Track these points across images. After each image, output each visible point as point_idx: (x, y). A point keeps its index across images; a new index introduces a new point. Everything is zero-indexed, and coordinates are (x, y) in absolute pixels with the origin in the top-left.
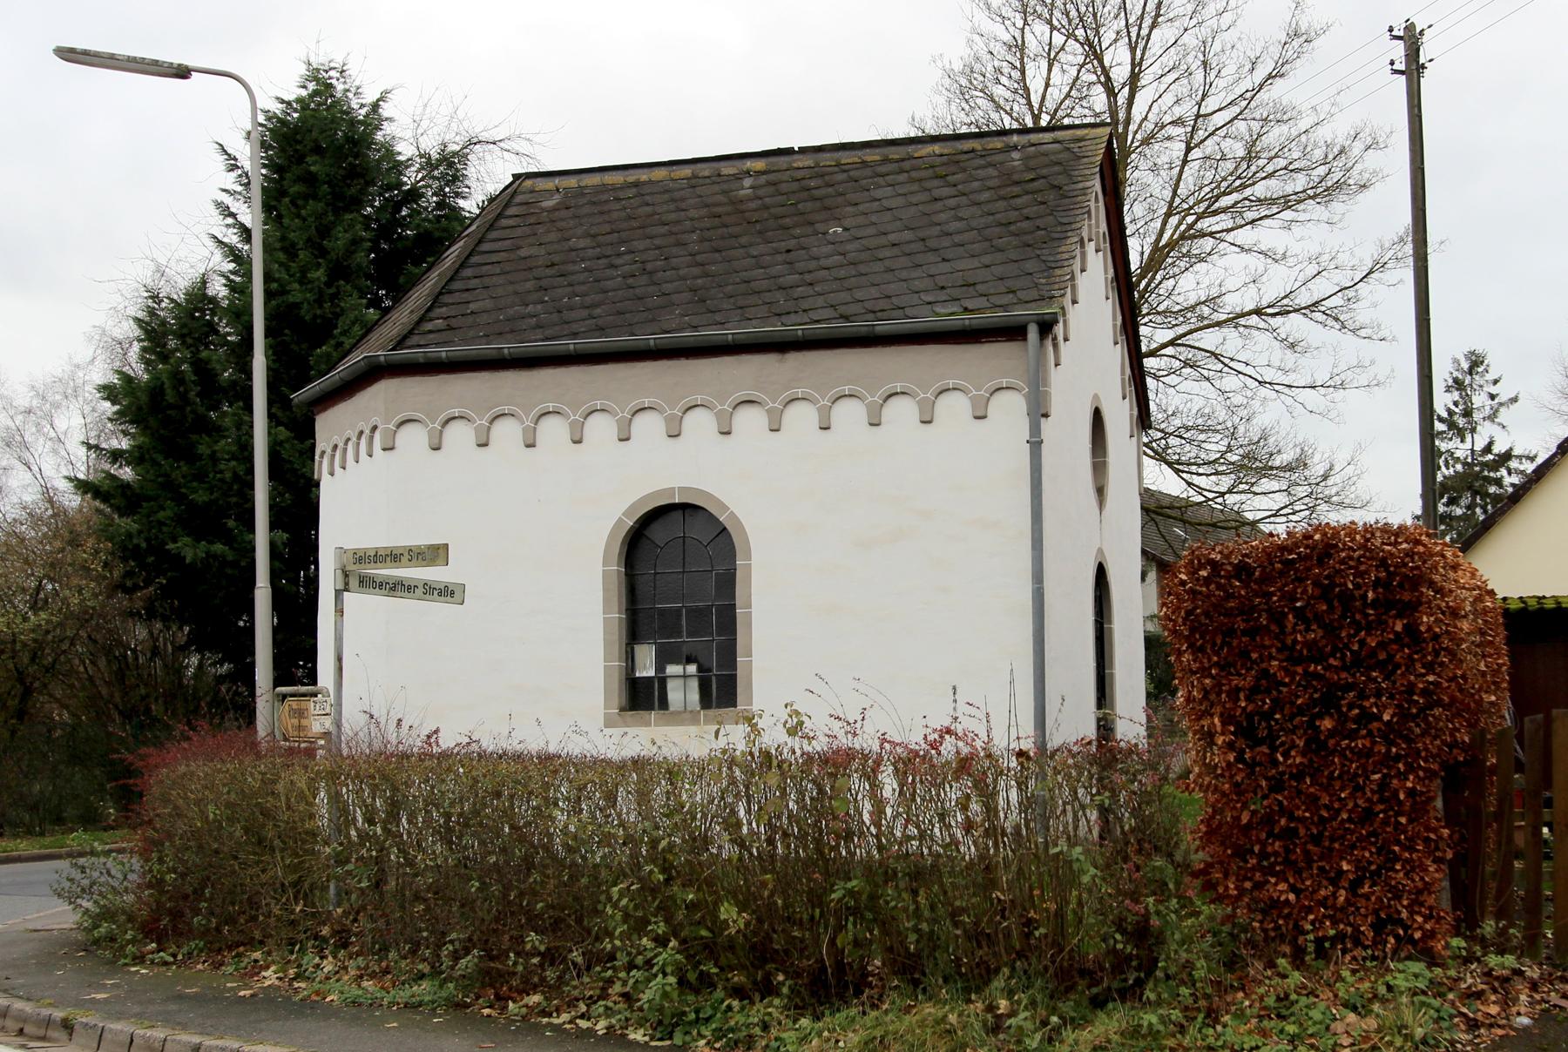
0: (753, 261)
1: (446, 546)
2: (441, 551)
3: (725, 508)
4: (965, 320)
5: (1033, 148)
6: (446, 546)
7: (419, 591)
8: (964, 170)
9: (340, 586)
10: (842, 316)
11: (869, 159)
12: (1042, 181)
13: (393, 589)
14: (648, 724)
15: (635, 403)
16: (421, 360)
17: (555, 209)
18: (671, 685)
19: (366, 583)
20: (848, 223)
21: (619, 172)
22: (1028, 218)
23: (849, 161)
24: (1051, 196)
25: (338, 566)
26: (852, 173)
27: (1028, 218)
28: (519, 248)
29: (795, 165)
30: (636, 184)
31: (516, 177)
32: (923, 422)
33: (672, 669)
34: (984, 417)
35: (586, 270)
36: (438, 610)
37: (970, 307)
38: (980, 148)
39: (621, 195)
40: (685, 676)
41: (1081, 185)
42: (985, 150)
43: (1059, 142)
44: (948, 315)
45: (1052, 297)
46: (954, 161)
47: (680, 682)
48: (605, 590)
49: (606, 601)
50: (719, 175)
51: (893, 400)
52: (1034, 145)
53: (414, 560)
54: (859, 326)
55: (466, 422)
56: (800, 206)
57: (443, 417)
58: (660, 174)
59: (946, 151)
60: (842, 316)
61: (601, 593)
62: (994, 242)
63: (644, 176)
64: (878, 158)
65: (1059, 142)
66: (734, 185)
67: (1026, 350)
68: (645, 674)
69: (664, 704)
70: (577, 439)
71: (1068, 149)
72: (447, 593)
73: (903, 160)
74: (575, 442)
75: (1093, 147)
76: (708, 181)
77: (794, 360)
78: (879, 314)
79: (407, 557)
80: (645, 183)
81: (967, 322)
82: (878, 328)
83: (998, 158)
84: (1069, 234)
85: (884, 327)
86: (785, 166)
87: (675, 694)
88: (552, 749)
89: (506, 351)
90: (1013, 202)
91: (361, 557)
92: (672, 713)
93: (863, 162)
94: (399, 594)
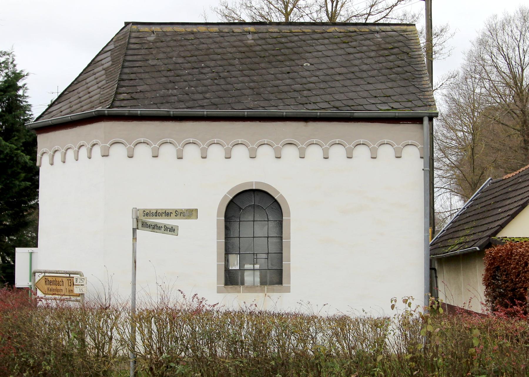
0: (273, 76)
1: (197, 210)
2: (194, 212)
3: (278, 193)
4: (392, 114)
5: (384, 33)
6: (197, 210)
7: (163, 229)
8: (356, 41)
9: (135, 227)
10: (334, 107)
11: (306, 31)
12: (397, 49)
13: (154, 228)
14: (239, 292)
15: (234, 141)
16: (127, 114)
17: (154, 42)
18: (246, 273)
19: (145, 225)
20: (311, 60)
21: (180, 26)
22: (399, 66)
23: (297, 31)
24: (405, 57)
25: (134, 217)
26: (300, 37)
27: (399, 66)
28: (147, 60)
29: (270, 30)
30: (192, 33)
31: (127, 24)
32: (372, 158)
33: (247, 266)
34: (400, 157)
35: (189, 74)
36: (168, 237)
37: (394, 107)
38: (358, 30)
39: (187, 37)
40: (254, 270)
41: (417, 53)
42: (361, 31)
43: (395, 31)
44: (383, 110)
45: (430, 105)
46: (348, 34)
47: (252, 272)
48: (218, 228)
49: (218, 233)
50: (233, 32)
51: (359, 147)
52: (384, 31)
53: (179, 216)
54: (346, 113)
55: (146, 145)
56: (282, 50)
57: (135, 142)
58: (202, 29)
59: (342, 31)
60: (334, 107)
61: (216, 230)
62: (389, 77)
63: (195, 29)
64: (310, 31)
65: (395, 31)
66: (244, 38)
67: (422, 128)
68: (234, 268)
69: (243, 283)
70: (204, 156)
71: (402, 35)
72: (172, 230)
73: (323, 33)
74: (203, 158)
75: (412, 35)
76: (228, 34)
77: (312, 126)
78: (352, 107)
79: (174, 214)
80: (196, 33)
81: (397, 114)
82: (355, 114)
83: (370, 36)
84: (423, 76)
85: (357, 114)
86: (265, 31)
87: (248, 278)
88: (297, 312)
89: (172, 113)
90: (388, 58)
91: (147, 213)
92: (247, 287)
93: (303, 32)
94: (156, 230)
